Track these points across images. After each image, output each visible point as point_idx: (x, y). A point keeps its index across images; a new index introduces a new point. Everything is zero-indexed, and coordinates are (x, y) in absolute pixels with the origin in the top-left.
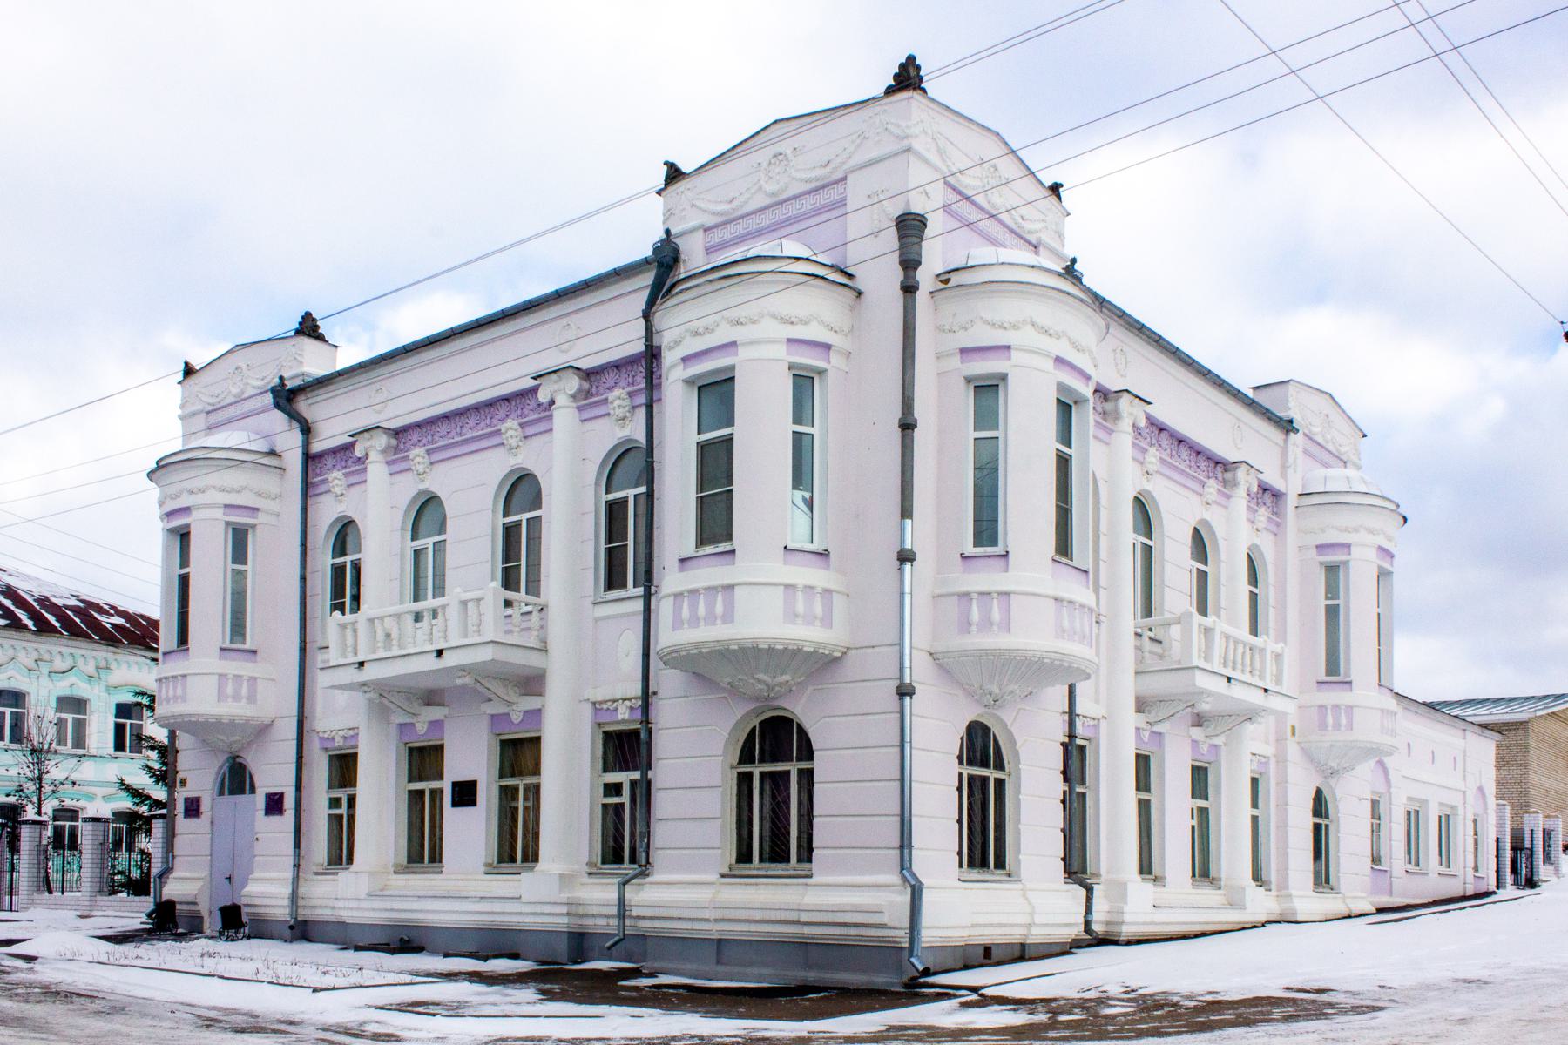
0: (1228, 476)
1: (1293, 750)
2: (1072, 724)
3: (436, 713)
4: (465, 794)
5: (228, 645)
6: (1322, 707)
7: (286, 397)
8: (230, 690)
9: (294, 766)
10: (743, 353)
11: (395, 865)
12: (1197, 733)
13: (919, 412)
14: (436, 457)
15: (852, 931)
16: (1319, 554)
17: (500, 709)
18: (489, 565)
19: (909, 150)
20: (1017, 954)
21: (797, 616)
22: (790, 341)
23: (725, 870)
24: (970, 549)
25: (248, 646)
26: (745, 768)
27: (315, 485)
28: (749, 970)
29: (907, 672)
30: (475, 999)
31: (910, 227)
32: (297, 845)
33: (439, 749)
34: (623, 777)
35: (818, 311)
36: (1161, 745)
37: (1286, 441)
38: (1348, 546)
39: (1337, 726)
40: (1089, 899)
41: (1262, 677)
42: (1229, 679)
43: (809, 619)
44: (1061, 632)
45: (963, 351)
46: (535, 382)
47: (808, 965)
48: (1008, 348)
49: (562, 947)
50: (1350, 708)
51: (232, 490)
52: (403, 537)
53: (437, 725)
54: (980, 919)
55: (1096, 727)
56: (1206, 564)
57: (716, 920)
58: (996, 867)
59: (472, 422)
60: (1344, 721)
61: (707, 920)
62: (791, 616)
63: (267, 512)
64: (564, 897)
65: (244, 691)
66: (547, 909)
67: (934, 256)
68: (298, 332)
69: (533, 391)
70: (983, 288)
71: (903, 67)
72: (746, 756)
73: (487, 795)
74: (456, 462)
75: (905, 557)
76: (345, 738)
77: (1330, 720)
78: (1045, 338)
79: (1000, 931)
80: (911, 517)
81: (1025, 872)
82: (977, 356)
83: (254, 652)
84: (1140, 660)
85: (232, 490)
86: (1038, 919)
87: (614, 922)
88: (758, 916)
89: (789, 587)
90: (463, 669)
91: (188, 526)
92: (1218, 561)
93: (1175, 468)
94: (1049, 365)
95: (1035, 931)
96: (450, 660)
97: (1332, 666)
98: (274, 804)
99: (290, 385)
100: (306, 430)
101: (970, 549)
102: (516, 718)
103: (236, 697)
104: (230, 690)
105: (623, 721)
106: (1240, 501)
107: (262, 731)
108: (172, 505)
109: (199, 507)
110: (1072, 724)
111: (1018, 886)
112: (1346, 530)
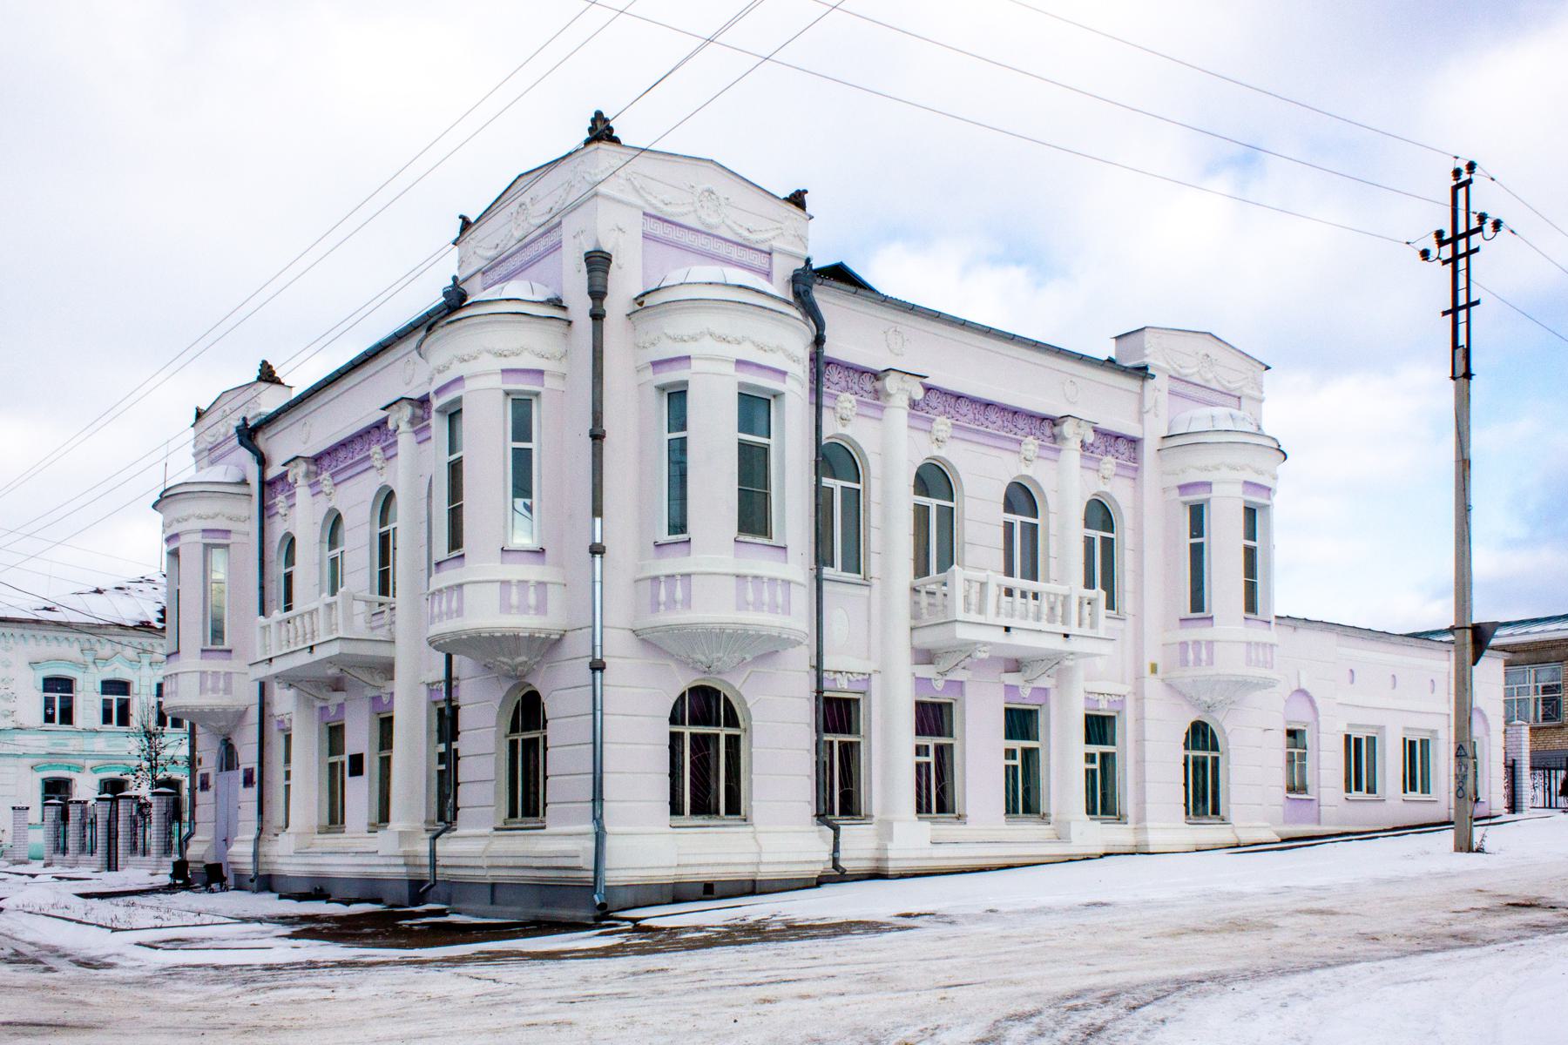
0: (1056, 430)
1: (1153, 685)
2: (819, 680)
3: (338, 697)
4: (357, 765)
5: (209, 646)
6: (1184, 644)
7: (248, 435)
8: (209, 684)
10: (469, 385)
11: (319, 826)
12: (1012, 679)
13: (607, 425)
14: (339, 478)
15: (563, 874)
16: (1181, 494)
17: (375, 693)
18: (367, 571)
19: (596, 195)
20: (748, 888)
21: (511, 607)
22: (504, 371)
23: (500, 824)
24: (664, 537)
25: (226, 646)
27: (270, 507)
29: (598, 649)
31: (598, 262)
32: (261, 811)
33: (342, 727)
35: (531, 345)
36: (962, 693)
37: (1142, 387)
38: (1208, 485)
39: (1198, 661)
40: (836, 838)
41: (1064, 622)
42: (1007, 629)
43: (523, 609)
44: (742, 605)
45: (655, 364)
46: (385, 413)
47: (544, 904)
48: (689, 358)
49: (405, 891)
50: (1210, 643)
51: (208, 517)
52: (321, 549)
53: (341, 707)
54: (684, 860)
55: (868, 680)
56: (1035, 515)
57: (491, 867)
58: (728, 812)
59: (358, 447)
60: (1204, 655)
61: (481, 867)
62: (506, 607)
63: (238, 533)
64: (401, 851)
65: (221, 684)
67: (624, 285)
68: (260, 379)
69: (385, 421)
70: (712, 304)
71: (594, 121)
72: (514, 728)
73: (371, 765)
74: (352, 481)
75: (597, 550)
77: (1191, 656)
78: (724, 345)
79: (695, 870)
80: (601, 515)
81: (756, 816)
82: (666, 367)
83: (230, 651)
84: (916, 615)
85: (208, 517)
86: (765, 858)
87: (427, 870)
88: (511, 862)
89: (505, 583)
90: (330, 661)
92: (1047, 512)
93: (989, 434)
94: (730, 368)
95: (763, 869)
96: (320, 654)
97: (1197, 603)
98: (248, 782)
99: (251, 424)
100: (262, 461)
101: (664, 537)
103: (214, 690)
104: (209, 684)
106: (1072, 454)
107: (241, 715)
108: (170, 532)
110: (819, 680)
111: (750, 829)
112: (1206, 469)
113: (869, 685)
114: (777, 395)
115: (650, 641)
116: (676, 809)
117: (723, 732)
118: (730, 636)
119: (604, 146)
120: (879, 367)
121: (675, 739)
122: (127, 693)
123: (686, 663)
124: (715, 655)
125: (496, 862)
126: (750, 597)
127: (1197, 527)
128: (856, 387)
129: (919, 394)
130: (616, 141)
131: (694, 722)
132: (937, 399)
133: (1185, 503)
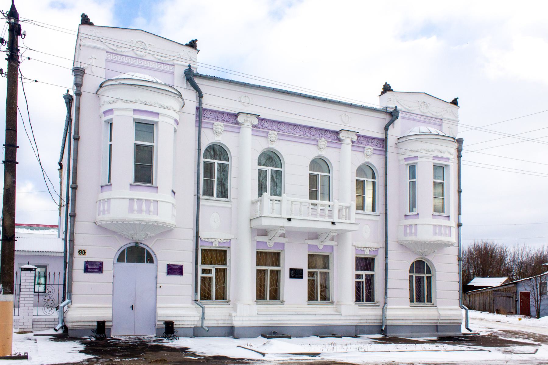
9: (389, 277)
26: (411, 274)
28: (422, 334)
30: (325, 351)
34: (364, 273)
41: (330, 216)
44: (435, 234)
66: (352, 318)
72: (411, 271)
76: (219, 243)
88: (426, 318)
91: (112, 119)
94: (131, 113)
102: (321, 247)
105: (367, 255)
106: (347, 147)
109: (119, 109)
113: (230, 245)
114: (157, 123)
115: (403, 246)
116: (411, 301)
117: (425, 276)
118: (428, 244)
119: (388, 93)
120: (338, 130)
121: (411, 277)
122: (224, 262)
123: (414, 252)
124: (426, 250)
125: (418, 318)
126: (437, 231)
127: (413, 175)
128: (276, 129)
129: (355, 138)
130: (392, 90)
131: (416, 273)
132: (263, 124)
133: (407, 165)
